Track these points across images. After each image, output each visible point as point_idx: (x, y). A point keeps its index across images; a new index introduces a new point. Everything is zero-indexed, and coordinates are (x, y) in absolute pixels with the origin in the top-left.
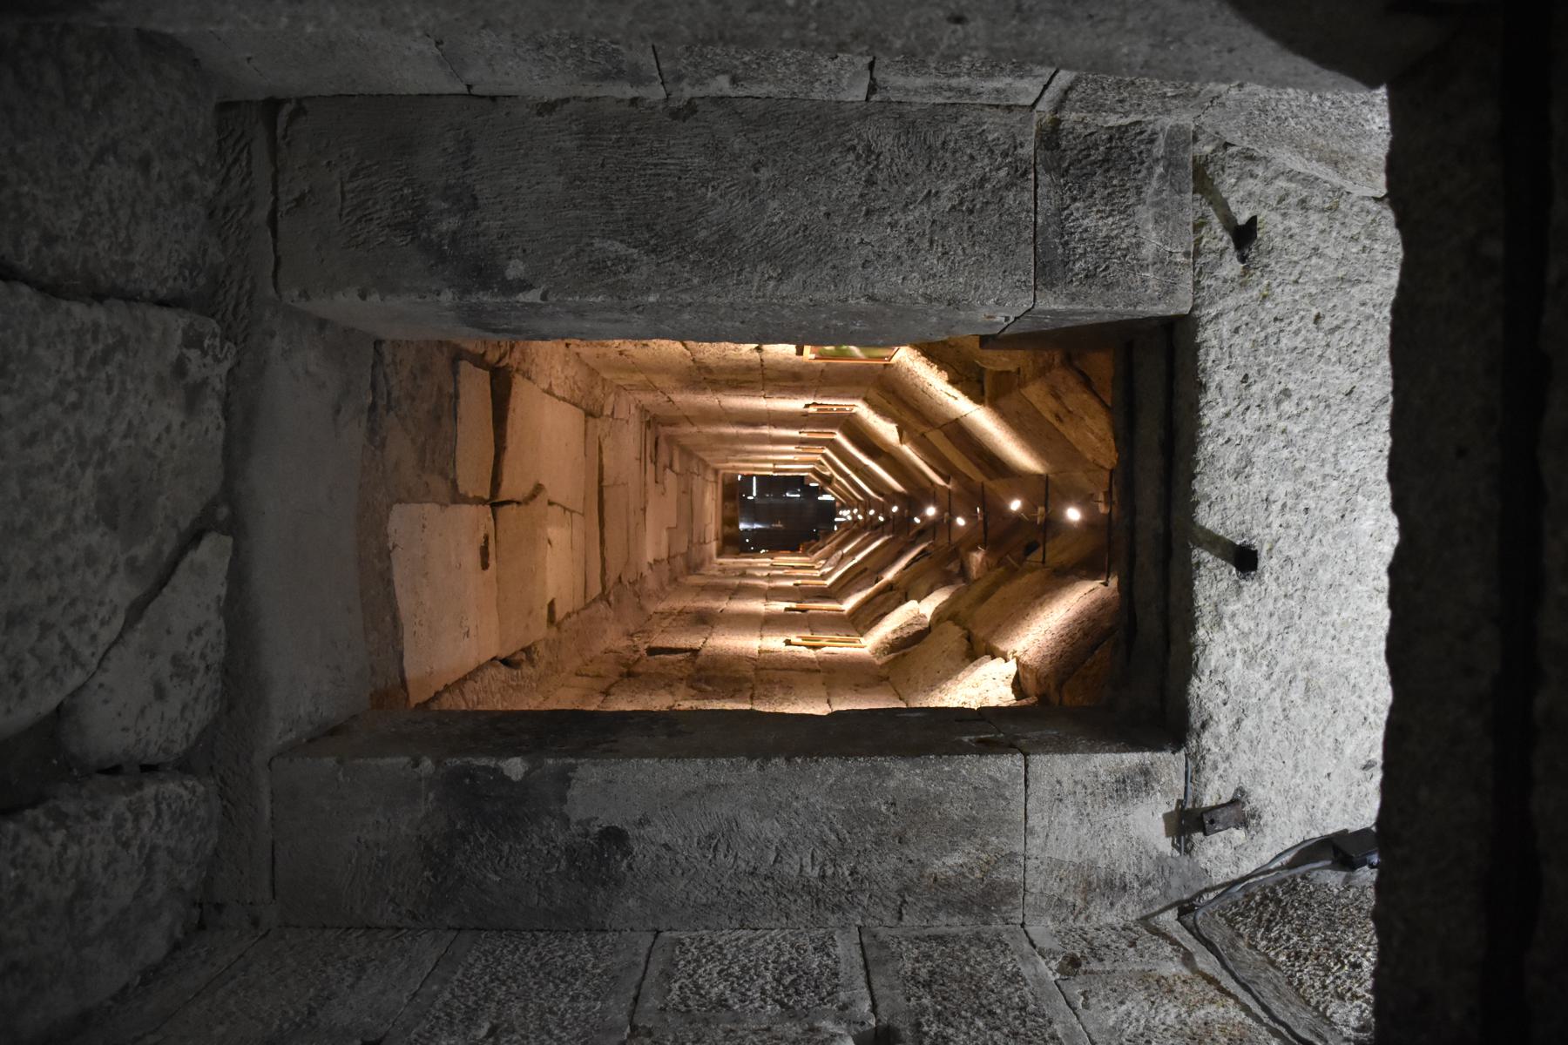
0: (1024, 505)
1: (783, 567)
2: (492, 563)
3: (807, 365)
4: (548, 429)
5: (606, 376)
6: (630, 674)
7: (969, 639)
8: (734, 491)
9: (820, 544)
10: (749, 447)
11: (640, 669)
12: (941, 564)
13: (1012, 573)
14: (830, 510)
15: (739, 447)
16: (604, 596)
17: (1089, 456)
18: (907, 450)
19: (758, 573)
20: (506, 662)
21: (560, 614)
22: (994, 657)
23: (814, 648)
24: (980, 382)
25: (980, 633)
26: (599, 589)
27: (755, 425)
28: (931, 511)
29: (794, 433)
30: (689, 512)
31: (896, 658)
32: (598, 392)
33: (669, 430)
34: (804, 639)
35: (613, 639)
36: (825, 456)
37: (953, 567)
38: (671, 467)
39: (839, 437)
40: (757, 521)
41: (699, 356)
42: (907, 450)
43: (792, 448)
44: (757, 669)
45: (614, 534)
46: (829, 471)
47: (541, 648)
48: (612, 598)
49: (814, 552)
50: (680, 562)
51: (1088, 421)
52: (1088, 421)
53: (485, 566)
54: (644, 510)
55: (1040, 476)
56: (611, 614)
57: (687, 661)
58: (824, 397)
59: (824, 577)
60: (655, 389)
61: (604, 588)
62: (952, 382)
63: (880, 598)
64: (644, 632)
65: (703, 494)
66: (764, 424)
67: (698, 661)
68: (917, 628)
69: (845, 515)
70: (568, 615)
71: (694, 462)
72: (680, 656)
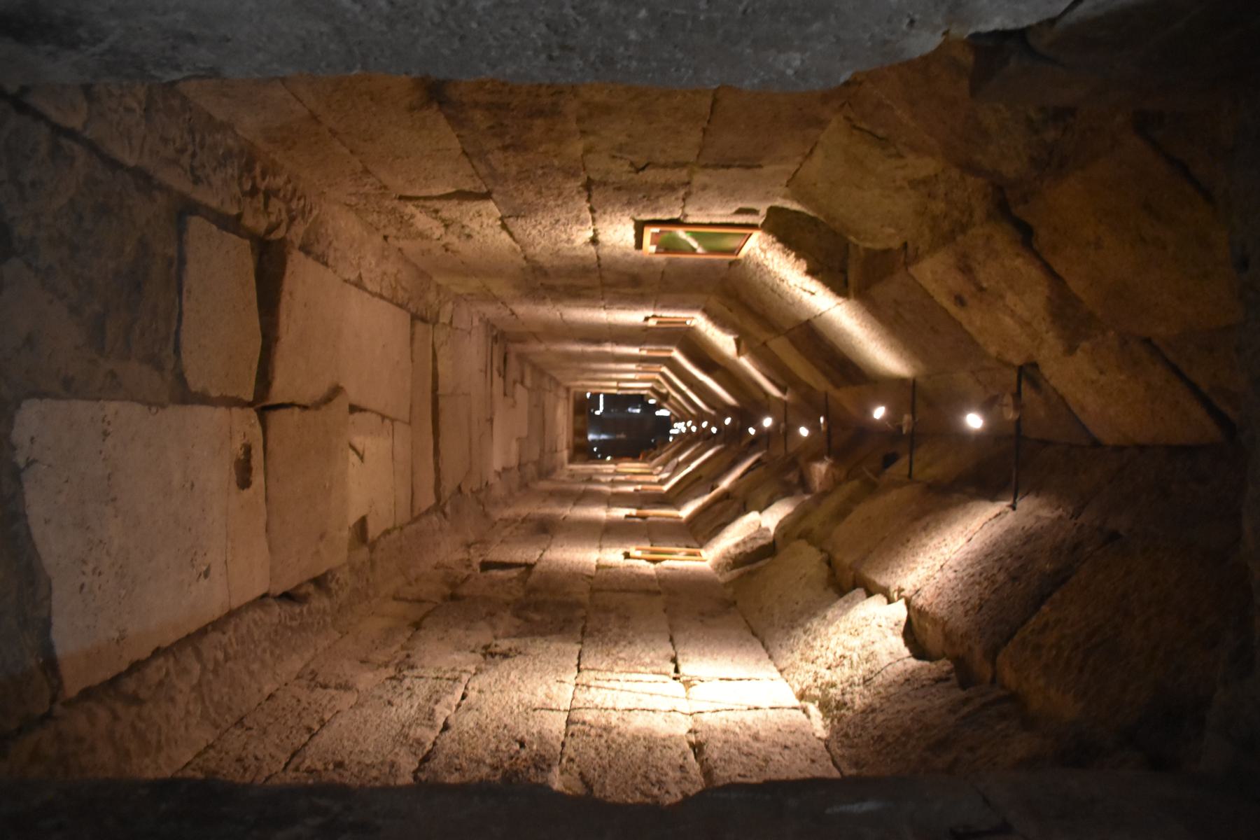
0: (889, 409)
2: (258, 479)
3: (648, 264)
4: (349, 323)
5: (442, 280)
6: (454, 597)
8: (583, 407)
9: (657, 452)
11: (464, 591)
12: (779, 474)
13: (871, 489)
14: (667, 423)
15: (585, 365)
16: (438, 507)
17: (993, 350)
18: (745, 362)
19: (603, 479)
20: (288, 597)
21: (373, 531)
22: (870, 594)
23: (654, 561)
24: (843, 271)
25: (845, 559)
26: (431, 501)
27: (598, 342)
28: (767, 422)
29: (634, 351)
30: (541, 424)
31: (741, 576)
32: (431, 297)
33: (518, 347)
35: (448, 552)
36: (663, 374)
37: (792, 477)
38: (522, 383)
39: (676, 354)
41: (565, 317)
42: (745, 362)
43: (632, 366)
44: (593, 591)
46: (666, 389)
47: (344, 575)
48: (448, 509)
49: (652, 459)
50: (531, 470)
51: (1010, 299)
52: (1010, 299)
53: (244, 482)
54: (491, 421)
55: (901, 381)
56: (447, 525)
57: (518, 579)
59: (662, 482)
60: (495, 299)
61: (438, 499)
62: (811, 272)
63: (719, 506)
64: (483, 542)
65: (555, 408)
66: (606, 341)
67: (532, 579)
68: (761, 542)
69: (679, 428)
70: (387, 532)
72: (514, 573)
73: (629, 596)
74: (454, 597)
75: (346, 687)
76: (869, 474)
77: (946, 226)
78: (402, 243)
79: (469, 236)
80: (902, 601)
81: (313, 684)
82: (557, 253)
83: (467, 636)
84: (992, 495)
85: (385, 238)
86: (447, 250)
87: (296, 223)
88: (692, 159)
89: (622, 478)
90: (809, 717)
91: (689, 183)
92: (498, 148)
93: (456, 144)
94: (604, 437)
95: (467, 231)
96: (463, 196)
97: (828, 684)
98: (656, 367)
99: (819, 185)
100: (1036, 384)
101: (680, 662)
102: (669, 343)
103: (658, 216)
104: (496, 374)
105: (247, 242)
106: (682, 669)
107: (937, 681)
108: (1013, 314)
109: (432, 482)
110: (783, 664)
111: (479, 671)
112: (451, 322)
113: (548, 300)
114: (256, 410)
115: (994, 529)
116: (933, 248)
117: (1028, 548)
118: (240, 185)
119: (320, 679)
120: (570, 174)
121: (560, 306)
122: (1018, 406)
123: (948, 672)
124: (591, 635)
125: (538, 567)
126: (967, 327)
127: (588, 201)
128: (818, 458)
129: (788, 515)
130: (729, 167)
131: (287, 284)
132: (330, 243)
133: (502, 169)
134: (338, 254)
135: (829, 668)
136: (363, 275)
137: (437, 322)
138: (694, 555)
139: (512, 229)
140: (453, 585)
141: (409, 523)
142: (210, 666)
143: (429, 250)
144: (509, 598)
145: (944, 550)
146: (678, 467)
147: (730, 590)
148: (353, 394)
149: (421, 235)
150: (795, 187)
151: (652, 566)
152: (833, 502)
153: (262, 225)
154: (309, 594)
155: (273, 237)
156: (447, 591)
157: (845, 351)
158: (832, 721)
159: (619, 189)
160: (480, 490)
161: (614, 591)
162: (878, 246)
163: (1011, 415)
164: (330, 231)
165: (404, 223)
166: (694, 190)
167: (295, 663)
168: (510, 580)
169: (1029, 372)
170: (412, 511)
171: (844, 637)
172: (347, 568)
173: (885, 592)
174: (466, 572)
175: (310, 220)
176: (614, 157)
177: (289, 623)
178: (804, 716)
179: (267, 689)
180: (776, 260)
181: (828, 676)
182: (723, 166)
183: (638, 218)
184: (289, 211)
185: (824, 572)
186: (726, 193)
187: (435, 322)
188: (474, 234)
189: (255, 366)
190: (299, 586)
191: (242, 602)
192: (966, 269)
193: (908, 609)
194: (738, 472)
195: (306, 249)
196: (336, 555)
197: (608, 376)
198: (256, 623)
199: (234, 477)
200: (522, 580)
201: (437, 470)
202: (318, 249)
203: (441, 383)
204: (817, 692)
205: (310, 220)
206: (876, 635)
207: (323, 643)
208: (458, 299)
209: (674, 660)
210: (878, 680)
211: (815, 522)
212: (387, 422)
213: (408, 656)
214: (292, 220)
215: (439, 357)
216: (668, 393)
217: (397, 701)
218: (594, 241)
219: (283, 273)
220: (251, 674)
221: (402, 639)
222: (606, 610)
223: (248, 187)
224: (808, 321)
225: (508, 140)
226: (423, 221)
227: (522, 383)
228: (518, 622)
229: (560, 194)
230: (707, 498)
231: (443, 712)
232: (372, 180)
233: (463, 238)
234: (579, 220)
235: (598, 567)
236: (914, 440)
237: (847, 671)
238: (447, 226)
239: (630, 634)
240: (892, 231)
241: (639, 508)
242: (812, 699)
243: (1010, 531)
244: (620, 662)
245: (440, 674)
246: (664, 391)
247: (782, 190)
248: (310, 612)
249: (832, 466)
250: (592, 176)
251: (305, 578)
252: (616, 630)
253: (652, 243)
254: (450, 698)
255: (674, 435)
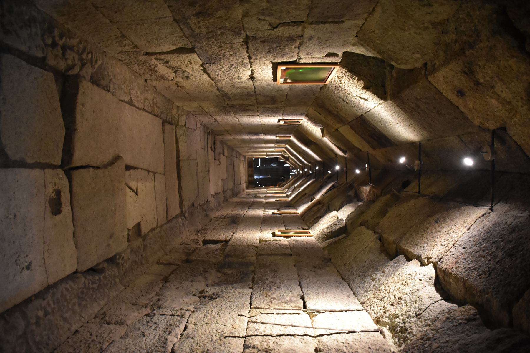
1: (271, 193)
2: (66, 209)
4: (122, 120)
5: (179, 104)
6: (188, 261)
7: (380, 240)
8: (252, 164)
9: (285, 183)
10: (256, 145)
11: (193, 258)
13: (397, 200)
14: (288, 170)
15: (252, 145)
16: (182, 214)
17: (477, 122)
18: (326, 140)
19: (261, 196)
20: (93, 270)
21: (144, 229)
22: (409, 259)
24: (383, 86)
26: (178, 211)
27: (257, 134)
29: (273, 137)
30: (233, 172)
31: (331, 244)
32: (174, 112)
34: (282, 232)
35: (188, 235)
36: (286, 148)
37: (351, 193)
38: (223, 154)
39: (293, 138)
40: (261, 175)
42: (326, 140)
43: (273, 145)
44: (258, 255)
45: (188, 184)
46: (288, 155)
48: (187, 215)
49: (283, 186)
50: (229, 193)
51: (499, 87)
52: (499, 87)
54: (208, 171)
55: (412, 144)
56: (186, 222)
58: (288, 114)
59: (288, 196)
60: (207, 113)
62: (366, 88)
63: (316, 208)
64: (205, 230)
65: (239, 165)
66: (260, 133)
67: (227, 250)
68: (340, 226)
71: (234, 153)
72: (219, 246)
73: (276, 257)
74: (188, 261)
75: (120, 323)
76: (395, 191)
77: (457, 47)
78: (155, 83)
79: (188, 77)
80: (431, 265)
81: (102, 321)
82: (233, 86)
83: (192, 286)
84: (476, 202)
85: (146, 80)
86: (178, 86)
87: (86, 66)
88: (304, 19)
89: (270, 195)
90: (385, 337)
91: (302, 36)
92: (193, 15)
93: (168, 13)
94: (261, 177)
95: (186, 74)
96: (181, 51)
97: (393, 315)
98: (283, 145)
99: (377, 31)
100: (503, 141)
101: (306, 299)
102: (290, 134)
103: (285, 60)
104: (210, 150)
105: (52, 74)
106: (308, 304)
107: (469, 320)
108: (498, 97)
109: (178, 202)
110: (363, 299)
111: (196, 309)
112: (185, 125)
113: (232, 114)
114: (65, 171)
115: (485, 223)
116: (446, 63)
117: (514, 236)
118: (43, 40)
119: (107, 318)
120: (237, 33)
121: (237, 116)
122: (494, 153)
123: (475, 315)
124: (257, 283)
125: (230, 243)
126: (462, 109)
127: (247, 52)
128: (365, 184)
129: (352, 212)
130: (325, 23)
131: (80, 99)
132: (111, 80)
133: (197, 31)
134: (116, 86)
135: (392, 305)
136: (133, 99)
137: (178, 124)
138: (307, 233)
139: (209, 72)
140: (188, 254)
141: (165, 224)
142: (33, 321)
143: (169, 87)
144: (214, 260)
145: (453, 235)
146: (294, 191)
147: (326, 252)
148: (128, 159)
149: (163, 78)
150: (362, 37)
151: (286, 239)
152: (377, 206)
153: (62, 66)
154: (104, 268)
155: (70, 73)
156: (184, 257)
157: (381, 130)
158: (399, 340)
159: (263, 42)
160: (203, 205)
161: (268, 255)
162: (409, 67)
163: (489, 158)
164: (110, 73)
165: (153, 70)
166: (305, 40)
167: (95, 308)
168: (217, 250)
169: (499, 134)
170: (167, 217)
171: (398, 285)
172: (129, 251)
173: (419, 258)
174: (195, 246)
175: (97, 66)
176: (260, 19)
177: (91, 286)
178: (382, 336)
179: (74, 328)
180: (347, 83)
181: (393, 310)
182: (322, 23)
183: (274, 61)
184: (81, 60)
185: (378, 244)
186: (323, 42)
187: (177, 125)
188: (190, 76)
189: (61, 145)
190: (98, 264)
191: (58, 279)
192: (469, 72)
193: (436, 269)
194: (324, 191)
195: (95, 81)
196: (120, 246)
197: (262, 150)
198: (67, 289)
199: (49, 209)
200: (223, 249)
201: (181, 196)
202: (103, 83)
203: (181, 154)
204: (387, 320)
205: (97, 66)
206: (419, 286)
207: (113, 293)
208: (189, 114)
209: (302, 298)
210: (426, 315)
211: (368, 216)
212: (151, 174)
213: (159, 300)
214: (83, 65)
215: (179, 141)
216: (289, 156)
217: (147, 332)
218: (252, 77)
219: (77, 93)
220: (65, 320)
221: (157, 289)
222: (265, 266)
223: (49, 41)
224: (362, 115)
225: (198, 9)
226: (162, 69)
227: (223, 154)
228: (219, 275)
229: (232, 47)
230: (310, 204)
231: (173, 340)
232: (128, 42)
233: (185, 78)
234: (244, 65)
235: (260, 241)
236: (419, 174)
237: (405, 309)
238: (175, 72)
239: (278, 281)
240: (419, 56)
241: (278, 210)
242: (385, 324)
243: (496, 224)
244: (274, 301)
245: (174, 312)
246: (287, 156)
247: (353, 39)
248: (105, 278)
249: (372, 187)
250: (248, 34)
251: (102, 259)
252: (270, 279)
253: (281, 78)
254: (177, 329)
255: (292, 175)
